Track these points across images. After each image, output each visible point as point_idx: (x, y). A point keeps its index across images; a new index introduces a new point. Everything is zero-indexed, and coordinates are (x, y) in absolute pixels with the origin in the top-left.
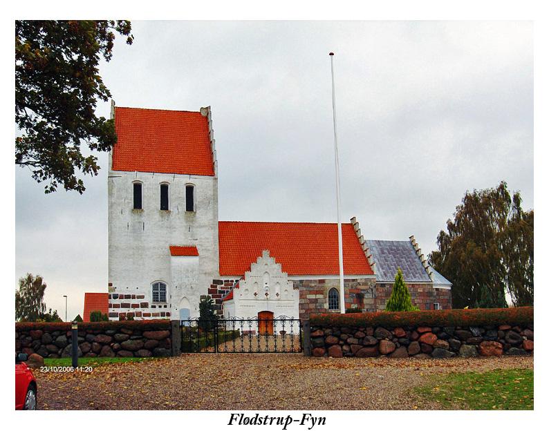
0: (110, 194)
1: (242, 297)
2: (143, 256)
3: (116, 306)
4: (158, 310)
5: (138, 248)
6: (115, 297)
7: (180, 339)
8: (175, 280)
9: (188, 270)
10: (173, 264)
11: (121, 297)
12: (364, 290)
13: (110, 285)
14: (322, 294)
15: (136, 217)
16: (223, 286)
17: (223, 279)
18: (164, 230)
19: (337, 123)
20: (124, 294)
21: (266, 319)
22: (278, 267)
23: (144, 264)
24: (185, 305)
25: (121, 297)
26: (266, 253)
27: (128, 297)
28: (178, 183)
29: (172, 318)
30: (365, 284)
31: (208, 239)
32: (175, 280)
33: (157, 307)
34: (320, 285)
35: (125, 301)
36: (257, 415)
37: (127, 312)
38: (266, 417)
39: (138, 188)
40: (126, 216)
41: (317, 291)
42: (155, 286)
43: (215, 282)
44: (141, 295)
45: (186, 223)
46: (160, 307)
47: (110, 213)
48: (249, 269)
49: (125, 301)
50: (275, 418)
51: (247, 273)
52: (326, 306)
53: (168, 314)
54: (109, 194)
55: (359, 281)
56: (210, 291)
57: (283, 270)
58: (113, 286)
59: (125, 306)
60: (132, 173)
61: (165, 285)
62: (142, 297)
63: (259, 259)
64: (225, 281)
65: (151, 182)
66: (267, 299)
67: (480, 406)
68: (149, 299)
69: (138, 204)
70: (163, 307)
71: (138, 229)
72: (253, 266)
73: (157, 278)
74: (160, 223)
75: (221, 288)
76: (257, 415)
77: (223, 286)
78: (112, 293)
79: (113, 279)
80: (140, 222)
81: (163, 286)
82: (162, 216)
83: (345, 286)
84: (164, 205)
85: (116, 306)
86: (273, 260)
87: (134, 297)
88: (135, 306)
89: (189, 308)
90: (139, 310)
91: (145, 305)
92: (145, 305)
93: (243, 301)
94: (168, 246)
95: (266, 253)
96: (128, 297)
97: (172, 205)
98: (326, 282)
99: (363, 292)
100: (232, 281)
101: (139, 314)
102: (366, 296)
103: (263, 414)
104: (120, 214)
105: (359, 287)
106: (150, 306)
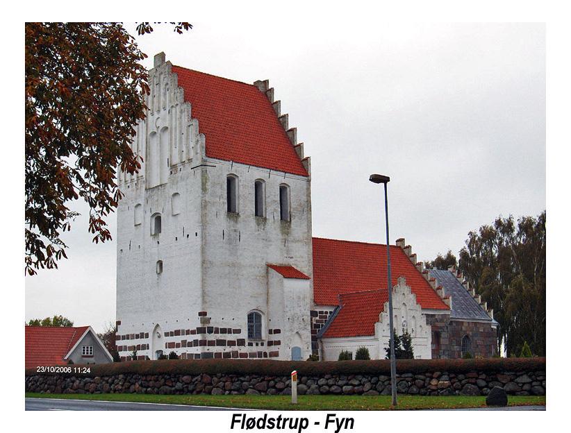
0: (204, 189)
2: (239, 277)
4: (255, 349)
5: (233, 265)
7: (199, 347)
8: (287, 309)
9: (299, 298)
10: (286, 290)
13: (203, 314)
15: (232, 223)
16: (318, 318)
17: (318, 310)
18: (262, 245)
23: (240, 287)
24: (297, 342)
26: (402, 280)
27: (224, 331)
29: (279, 359)
30: (441, 321)
31: (302, 257)
32: (287, 309)
33: (254, 345)
35: (220, 336)
36: (266, 415)
37: (223, 351)
38: (279, 419)
40: (220, 222)
42: (250, 317)
45: (282, 234)
47: (204, 216)
49: (220, 336)
50: (288, 419)
53: (276, 354)
54: (202, 189)
55: (436, 317)
57: (418, 301)
58: (208, 316)
59: (221, 343)
60: (227, 162)
61: (260, 316)
62: (238, 331)
68: (244, 335)
70: (260, 345)
71: (233, 240)
73: (251, 307)
74: (257, 233)
76: (266, 415)
77: (318, 318)
78: (206, 326)
79: (207, 305)
80: (235, 231)
81: (259, 317)
82: (258, 224)
84: (258, 212)
87: (229, 331)
88: (231, 343)
89: (301, 347)
90: (236, 348)
91: (241, 342)
92: (241, 342)
94: (264, 263)
95: (402, 280)
96: (224, 331)
100: (326, 313)
101: (235, 354)
102: (442, 335)
103: (273, 414)
106: (247, 344)
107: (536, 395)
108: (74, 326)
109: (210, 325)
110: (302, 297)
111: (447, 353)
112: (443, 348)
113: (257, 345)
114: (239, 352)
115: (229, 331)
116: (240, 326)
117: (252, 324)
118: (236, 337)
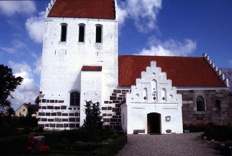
1: (134, 101)
3: (44, 108)
6: (44, 101)
11: (48, 101)
12: (220, 98)
14: (192, 100)
16: (121, 94)
19: (139, 102)
20: (50, 99)
21: (154, 120)
22: (164, 75)
25: (48, 101)
28: (91, 25)
30: (221, 93)
33: (73, 109)
34: (191, 94)
35: (50, 104)
39: (64, 28)
41: (188, 98)
43: (115, 91)
44: (62, 100)
46: (75, 109)
48: (140, 77)
49: (50, 104)
51: (138, 80)
52: (195, 109)
56: (111, 98)
58: (43, 94)
62: (62, 102)
63: (148, 68)
64: (122, 91)
65: (73, 24)
66: (155, 103)
67: (184, 122)
68: (67, 103)
69: (64, 38)
72: (143, 73)
75: (120, 96)
83: (76, 103)
84: (81, 38)
85: (44, 108)
86: (159, 69)
87: (56, 101)
91: (64, 108)
92: (64, 108)
93: (134, 104)
96: (52, 101)
97: (86, 38)
98: (194, 91)
99: (219, 99)
104: (50, 45)
105: (217, 95)
106: (67, 108)
107: (224, 107)
108: (31, 104)
109: (44, 98)
110: (95, 81)
111: (96, 104)
112: (223, 110)
113: (75, 109)
114: (62, 113)
115: (56, 101)
116: (64, 99)
117: (73, 98)
118: (61, 105)
